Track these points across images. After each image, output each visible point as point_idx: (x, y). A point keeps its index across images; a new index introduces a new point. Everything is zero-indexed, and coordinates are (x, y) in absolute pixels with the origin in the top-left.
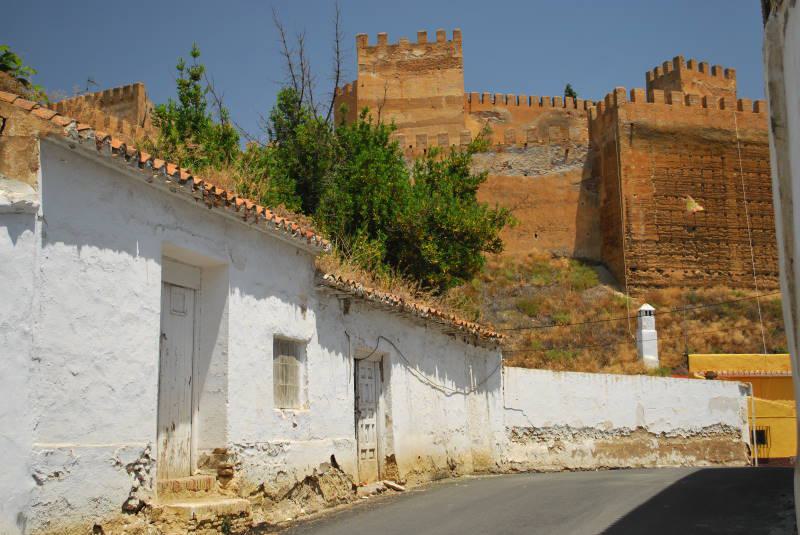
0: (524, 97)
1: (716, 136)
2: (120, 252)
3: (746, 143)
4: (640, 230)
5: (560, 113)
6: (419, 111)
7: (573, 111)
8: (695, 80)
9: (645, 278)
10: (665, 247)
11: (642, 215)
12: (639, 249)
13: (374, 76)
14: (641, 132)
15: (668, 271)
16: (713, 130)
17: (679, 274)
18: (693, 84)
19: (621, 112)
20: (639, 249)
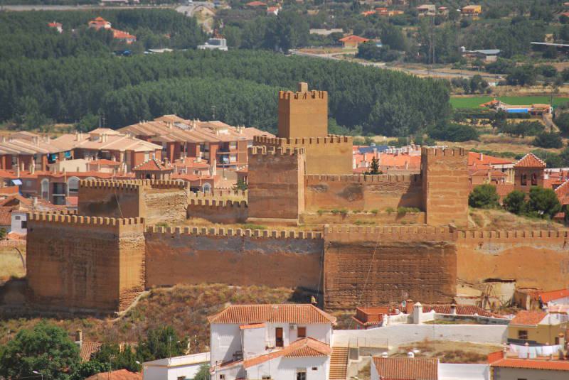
1: (369, 245)
2: (565, 70)
3: (384, 247)
4: (331, 286)
6: (277, 191)
7: (364, 183)
8: (438, 161)
9: (462, 173)
11: (332, 280)
12: (330, 294)
14: (337, 246)
15: (342, 303)
16: (368, 242)
17: (347, 304)
18: (437, 163)
20: (330, 294)
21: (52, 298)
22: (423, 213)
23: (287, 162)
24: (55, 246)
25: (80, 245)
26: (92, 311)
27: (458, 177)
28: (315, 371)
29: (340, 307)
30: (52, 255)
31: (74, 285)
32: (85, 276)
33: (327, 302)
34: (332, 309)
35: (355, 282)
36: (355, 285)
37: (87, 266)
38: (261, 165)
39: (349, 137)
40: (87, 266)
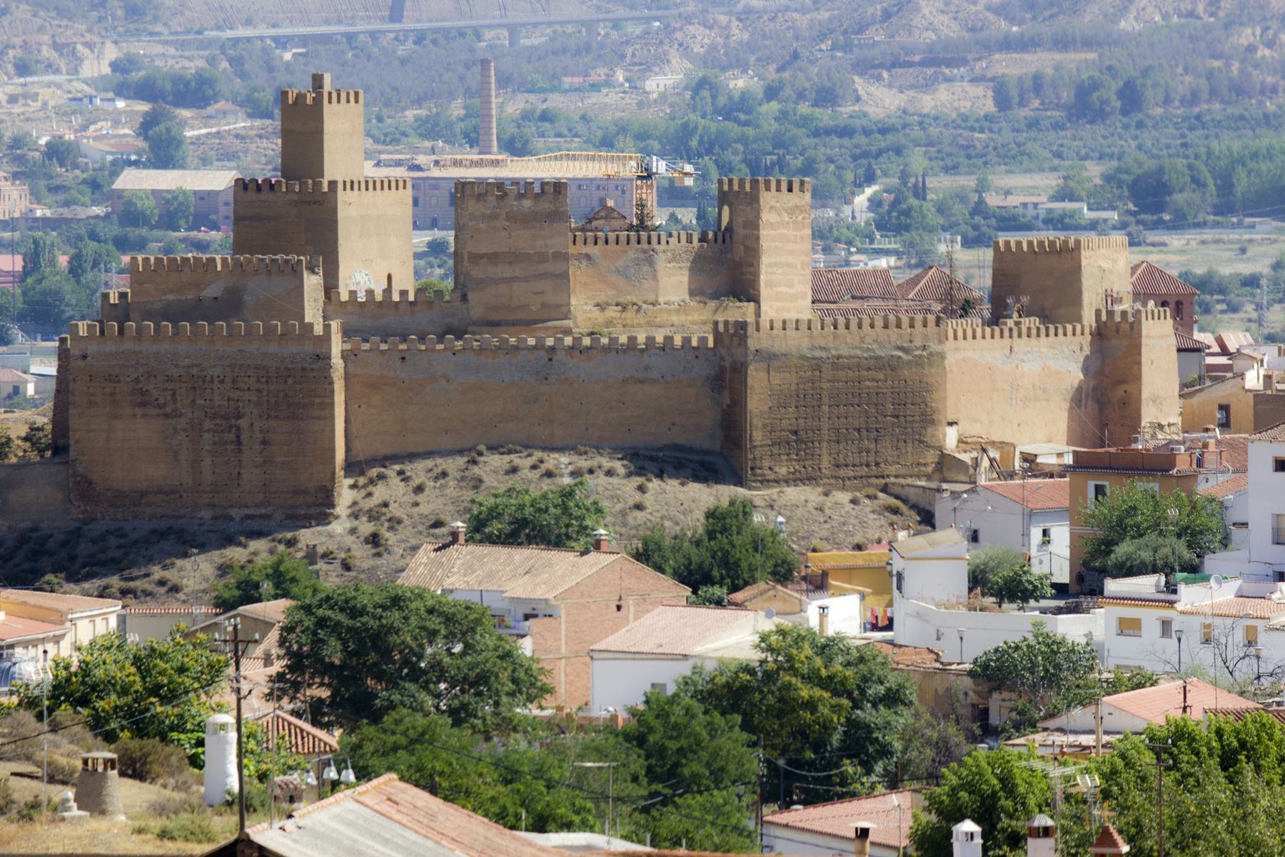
0: (612, 245)
4: (758, 436)
5: (645, 252)
10: (775, 450)
17: (783, 471)
19: (749, 341)
21: (143, 494)
22: (752, 304)
23: (545, 206)
24: (151, 387)
25: (222, 382)
26: (263, 511)
27: (798, 233)
28: (981, 536)
29: (772, 477)
30: (143, 404)
31: (207, 463)
32: (238, 442)
33: (752, 469)
34: (761, 482)
35: (794, 428)
36: (796, 433)
37: (243, 423)
38: (494, 217)
39: (806, 179)
40: (243, 423)
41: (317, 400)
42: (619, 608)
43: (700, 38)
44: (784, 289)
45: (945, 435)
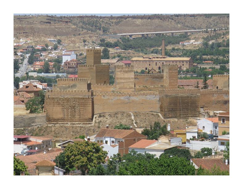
13: (119, 73)
17: (171, 116)
41: (88, 104)
42: (134, 140)
43: (205, 35)
44: (173, 84)
45: (200, 110)
